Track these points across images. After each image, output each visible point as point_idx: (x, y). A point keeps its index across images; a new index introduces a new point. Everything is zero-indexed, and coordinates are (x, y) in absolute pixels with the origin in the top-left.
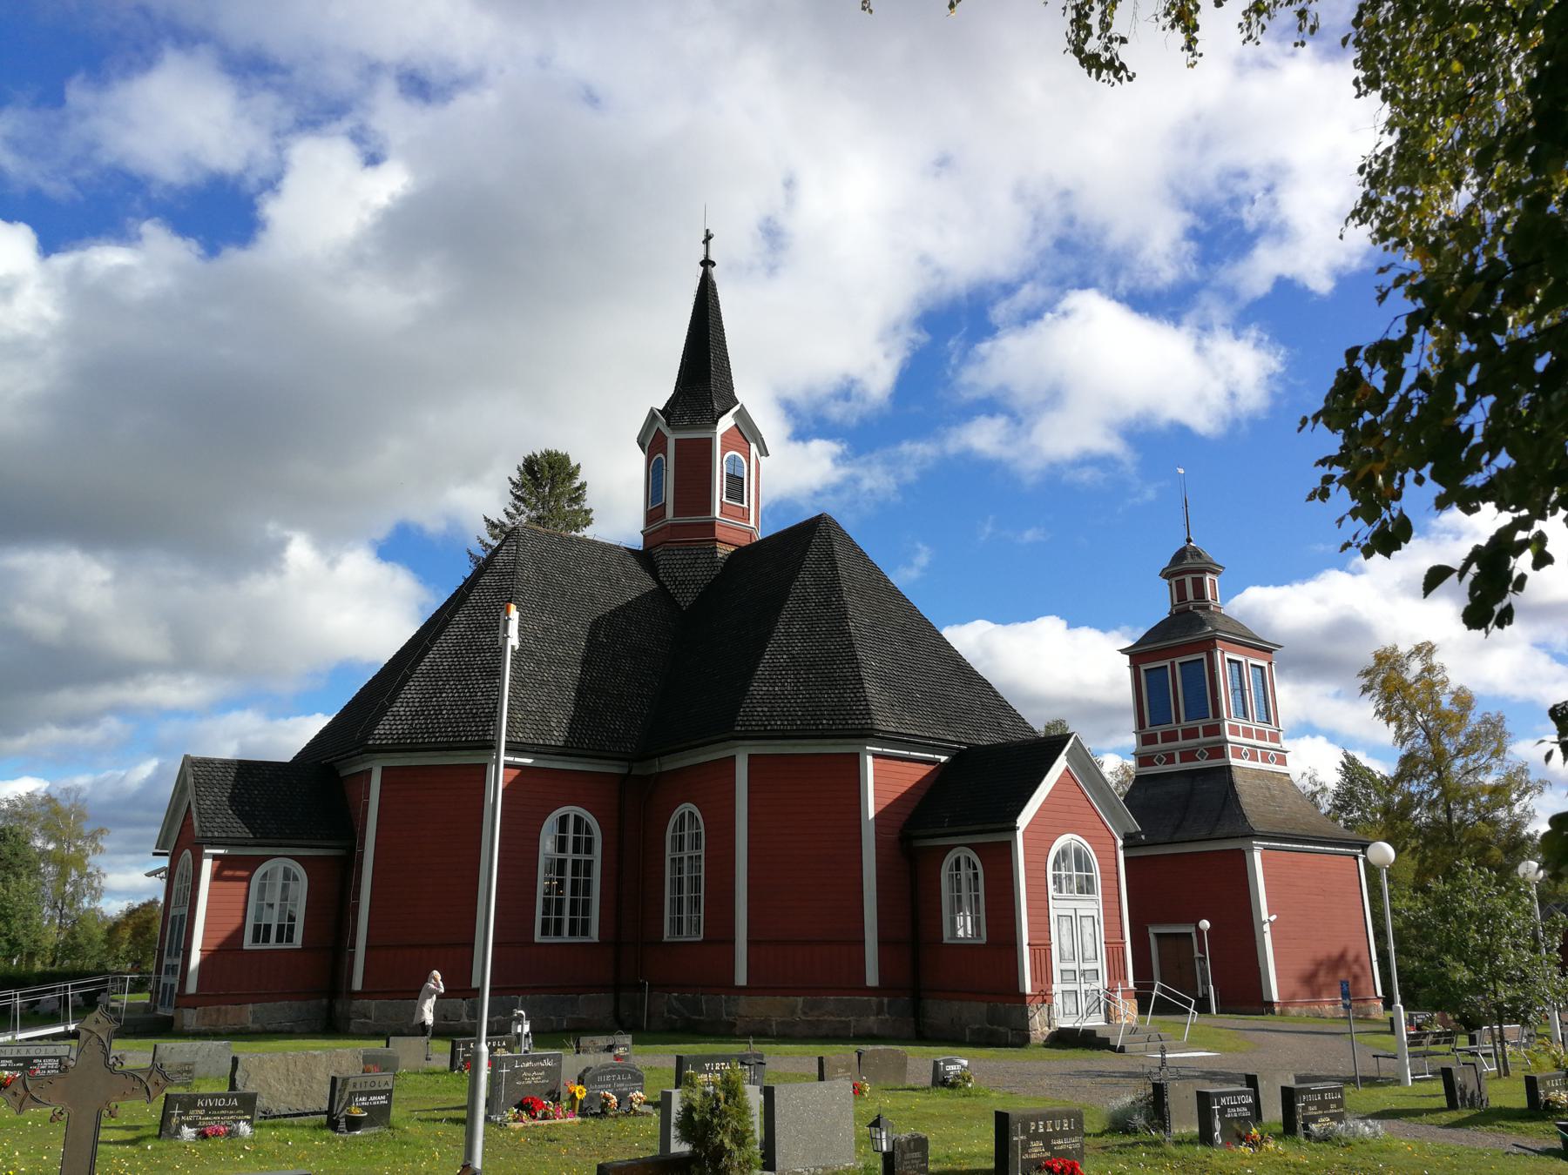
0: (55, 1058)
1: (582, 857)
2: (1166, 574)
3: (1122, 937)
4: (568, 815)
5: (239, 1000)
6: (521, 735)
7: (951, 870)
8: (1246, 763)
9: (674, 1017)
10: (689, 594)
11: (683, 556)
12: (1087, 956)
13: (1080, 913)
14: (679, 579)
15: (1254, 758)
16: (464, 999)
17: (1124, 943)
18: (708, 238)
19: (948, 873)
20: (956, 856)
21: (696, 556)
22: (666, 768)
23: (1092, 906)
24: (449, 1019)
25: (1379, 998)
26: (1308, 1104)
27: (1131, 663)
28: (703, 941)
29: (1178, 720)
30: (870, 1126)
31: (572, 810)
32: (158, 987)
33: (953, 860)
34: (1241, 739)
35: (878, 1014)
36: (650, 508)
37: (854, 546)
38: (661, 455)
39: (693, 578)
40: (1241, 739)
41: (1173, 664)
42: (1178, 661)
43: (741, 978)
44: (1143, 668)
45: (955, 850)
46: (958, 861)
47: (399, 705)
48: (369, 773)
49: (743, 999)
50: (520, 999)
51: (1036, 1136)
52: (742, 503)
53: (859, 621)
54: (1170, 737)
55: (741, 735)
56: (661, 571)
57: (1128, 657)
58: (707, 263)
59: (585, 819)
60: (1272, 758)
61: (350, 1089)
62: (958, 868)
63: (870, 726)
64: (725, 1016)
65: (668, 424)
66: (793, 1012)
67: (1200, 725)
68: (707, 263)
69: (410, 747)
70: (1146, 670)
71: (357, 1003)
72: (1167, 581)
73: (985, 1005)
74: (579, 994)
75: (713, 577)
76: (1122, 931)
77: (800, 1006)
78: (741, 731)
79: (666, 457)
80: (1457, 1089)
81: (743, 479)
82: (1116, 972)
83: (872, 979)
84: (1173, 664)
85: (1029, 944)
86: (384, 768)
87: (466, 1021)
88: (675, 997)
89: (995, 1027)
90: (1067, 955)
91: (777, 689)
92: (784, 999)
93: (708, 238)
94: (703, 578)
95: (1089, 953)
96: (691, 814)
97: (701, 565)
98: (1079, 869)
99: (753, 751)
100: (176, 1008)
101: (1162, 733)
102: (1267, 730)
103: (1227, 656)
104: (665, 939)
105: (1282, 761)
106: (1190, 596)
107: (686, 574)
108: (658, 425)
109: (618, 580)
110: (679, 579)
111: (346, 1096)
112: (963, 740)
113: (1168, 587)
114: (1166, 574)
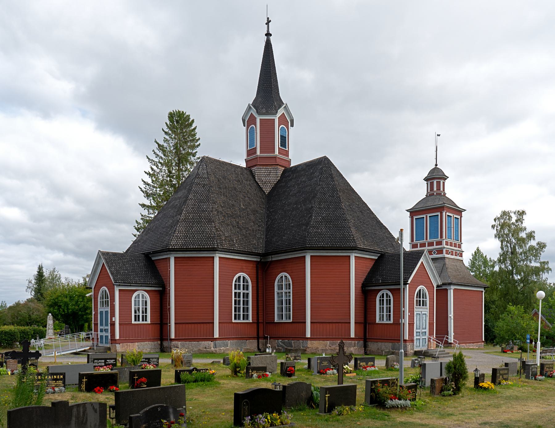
0: (156, 358)
1: (246, 291)
2: (426, 179)
3: (433, 321)
4: (241, 276)
5: (133, 341)
6: (226, 246)
7: (380, 298)
8: (449, 256)
9: (280, 348)
10: (268, 188)
11: (265, 171)
12: (423, 327)
13: (423, 313)
14: (264, 181)
15: (452, 255)
16: (212, 342)
17: (434, 323)
18: (268, 22)
19: (379, 299)
20: (382, 293)
21: (270, 171)
22: (274, 259)
23: (425, 310)
24: (207, 348)
25: (483, 341)
26: (547, 368)
27: (410, 216)
28: (393, 323)
29: (427, 239)
30: (474, 371)
31: (242, 274)
32: (97, 337)
33: (381, 294)
34: (449, 247)
35: (354, 347)
36: (249, 149)
37: (338, 171)
38: (253, 126)
39: (269, 181)
40: (449, 247)
41: (427, 216)
42: (428, 215)
43: (308, 335)
44: (415, 218)
45: (382, 291)
46: (383, 295)
47: (177, 232)
48: (169, 259)
49: (309, 342)
50: (229, 342)
51: (501, 374)
52: (286, 148)
53: (344, 205)
54: (423, 245)
55: (309, 248)
56: (256, 177)
57: (409, 213)
58: (268, 35)
59: (246, 278)
60: (458, 254)
61: (286, 366)
62: (383, 297)
63: (355, 246)
64: (302, 348)
65: (257, 112)
66: (326, 346)
67: (434, 240)
68: (268, 35)
69: (186, 250)
70: (416, 219)
71: (174, 342)
72: (426, 182)
73: (391, 344)
74: (247, 340)
75: (277, 181)
76: (434, 319)
77: (328, 344)
78: (309, 247)
79: (256, 127)
80: (98, 413)
81: (286, 137)
82: (431, 333)
83: (353, 335)
84: (427, 216)
85: (409, 324)
86: (311, 256)
87: (213, 349)
88: (281, 342)
89: (394, 351)
90: (418, 327)
91: (319, 230)
92: (323, 342)
93: (268, 22)
94: (273, 181)
95: (424, 327)
96: (286, 276)
97: (272, 175)
98: (247, 283)
99: (313, 254)
100: (111, 344)
101: (420, 244)
102: (449, 241)
103: (447, 214)
104: (276, 321)
105: (461, 256)
106: (435, 189)
107: (266, 179)
108: (251, 112)
109: (242, 181)
110: (264, 181)
111: (286, 368)
112: (383, 251)
113: (426, 185)
114: (426, 179)
